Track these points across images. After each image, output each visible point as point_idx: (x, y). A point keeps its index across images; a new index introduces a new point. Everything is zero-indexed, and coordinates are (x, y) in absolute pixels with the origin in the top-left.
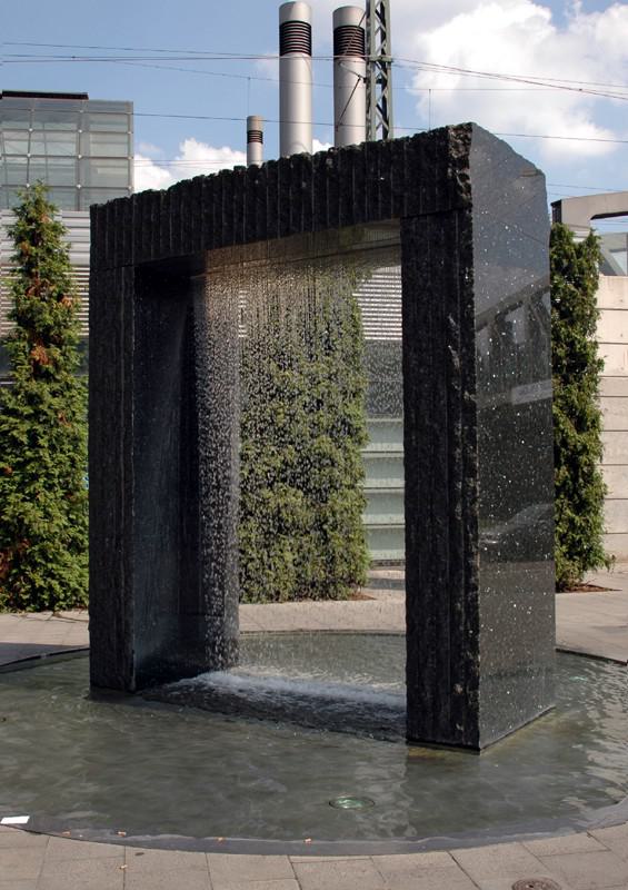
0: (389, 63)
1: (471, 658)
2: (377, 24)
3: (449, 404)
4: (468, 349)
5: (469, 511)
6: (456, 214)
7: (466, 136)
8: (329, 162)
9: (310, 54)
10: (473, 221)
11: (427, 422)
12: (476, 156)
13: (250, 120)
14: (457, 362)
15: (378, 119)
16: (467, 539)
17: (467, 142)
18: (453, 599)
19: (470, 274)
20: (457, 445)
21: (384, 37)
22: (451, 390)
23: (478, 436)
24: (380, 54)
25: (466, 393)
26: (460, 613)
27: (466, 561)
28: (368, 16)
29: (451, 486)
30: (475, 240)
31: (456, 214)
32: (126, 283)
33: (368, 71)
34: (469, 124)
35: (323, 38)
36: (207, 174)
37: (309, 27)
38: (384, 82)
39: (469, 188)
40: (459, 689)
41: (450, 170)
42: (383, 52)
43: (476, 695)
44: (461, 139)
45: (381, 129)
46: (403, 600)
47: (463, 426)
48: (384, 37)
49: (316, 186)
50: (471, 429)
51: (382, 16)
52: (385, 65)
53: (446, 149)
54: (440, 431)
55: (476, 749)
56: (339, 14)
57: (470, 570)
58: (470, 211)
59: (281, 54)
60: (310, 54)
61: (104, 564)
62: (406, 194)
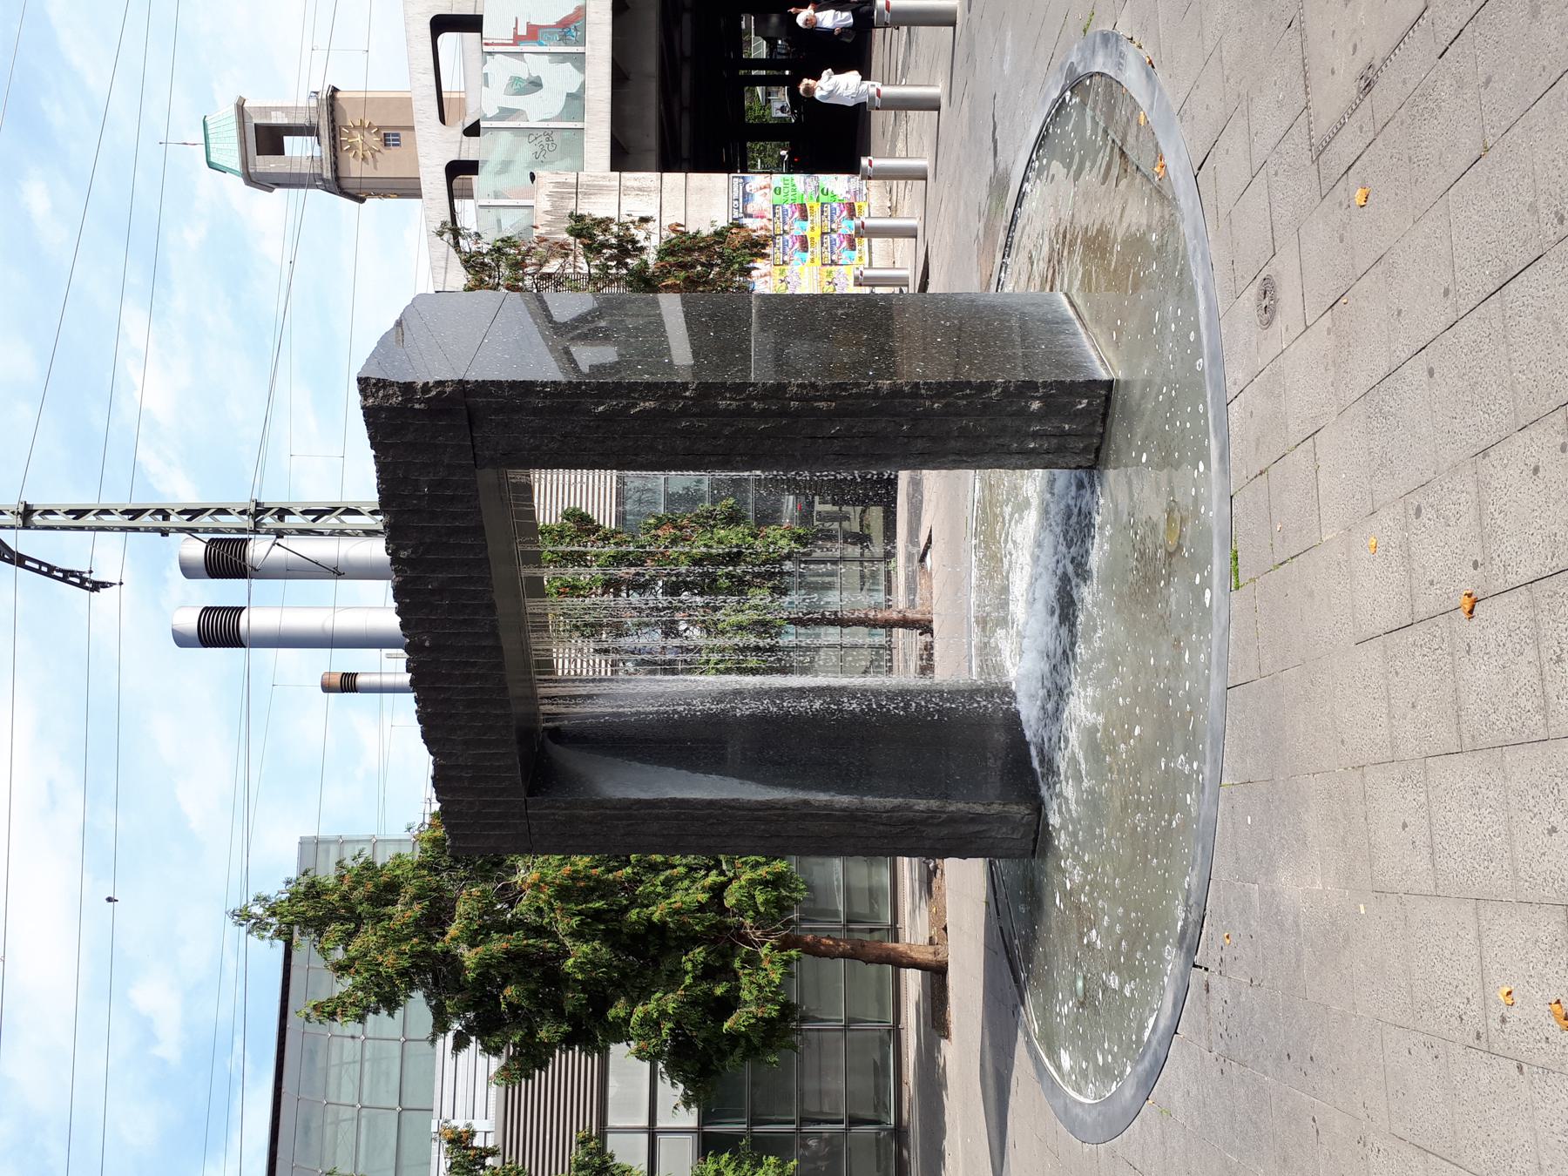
0: (258, 504)
1: (1000, 390)
2: (205, 521)
3: (700, 415)
4: (635, 391)
5: (827, 393)
6: (471, 400)
7: (375, 385)
8: (403, 554)
9: (241, 609)
10: (480, 379)
11: (722, 441)
12: (399, 374)
13: (327, 688)
14: (650, 404)
15: (331, 521)
16: (859, 396)
17: (382, 384)
18: (929, 413)
19: (544, 385)
20: (748, 406)
21: (222, 511)
22: (684, 412)
23: (738, 381)
24: (245, 517)
25: (687, 394)
26: (946, 405)
27: (885, 397)
28: (195, 530)
29: (797, 414)
30: (503, 377)
31: (471, 400)
32: (547, 808)
33: (268, 532)
34: (359, 380)
35: (225, 592)
36: (415, 707)
37: (206, 609)
38: (282, 513)
39: (439, 383)
40: (1035, 405)
41: (417, 406)
42: (243, 512)
43: (1045, 384)
44: (377, 392)
45: (343, 517)
46: (932, 479)
47: (725, 398)
48: (222, 511)
49: (433, 571)
50: (728, 389)
51: (195, 513)
52: (260, 511)
53: (391, 409)
54: (732, 426)
55: (1109, 384)
56: (188, 571)
57: (896, 392)
58: (468, 382)
59: (242, 646)
60: (241, 609)
61: (886, 837)
62: (446, 461)
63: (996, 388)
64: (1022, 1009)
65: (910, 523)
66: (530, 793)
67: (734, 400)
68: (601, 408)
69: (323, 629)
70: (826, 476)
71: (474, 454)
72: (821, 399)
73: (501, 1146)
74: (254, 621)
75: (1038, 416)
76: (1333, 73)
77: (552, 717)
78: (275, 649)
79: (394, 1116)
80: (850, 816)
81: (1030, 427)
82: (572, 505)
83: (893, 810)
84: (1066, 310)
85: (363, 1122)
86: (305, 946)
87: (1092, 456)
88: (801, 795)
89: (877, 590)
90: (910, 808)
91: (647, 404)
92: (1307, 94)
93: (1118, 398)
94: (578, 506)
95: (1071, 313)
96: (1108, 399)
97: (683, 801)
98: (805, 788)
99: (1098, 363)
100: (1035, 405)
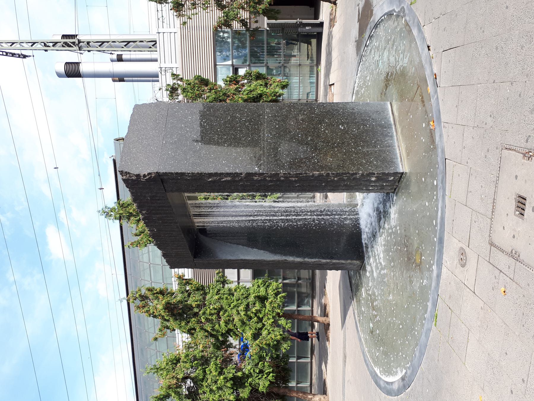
1: (360, 175)
37: (67, 63)
40: (373, 179)
63: (359, 174)
64: (353, 302)
65: (326, 66)
66: (195, 257)
67: (260, 177)
68: (210, 179)
69: (110, 72)
70: (295, 172)
71: (164, 186)
72: (292, 177)
73: (193, 278)
74: (83, 68)
75: (374, 182)
76: (507, 214)
77: (198, 226)
78: (94, 78)
79: (161, 266)
80: (301, 263)
81: (371, 184)
82: (198, 74)
83: (314, 262)
84: (390, 117)
85: (152, 268)
86: (124, 222)
87: (393, 190)
88: (284, 258)
89: (313, 77)
90: (320, 261)
91: (227, 178)
92: (493, 215)
93: (404, 180)
94: (200, 75)
95: (392, 122)
96: (401, 177)
97: (245, 260)
98: (285, 255)
99: (399, 159)
100: (373, 179)
